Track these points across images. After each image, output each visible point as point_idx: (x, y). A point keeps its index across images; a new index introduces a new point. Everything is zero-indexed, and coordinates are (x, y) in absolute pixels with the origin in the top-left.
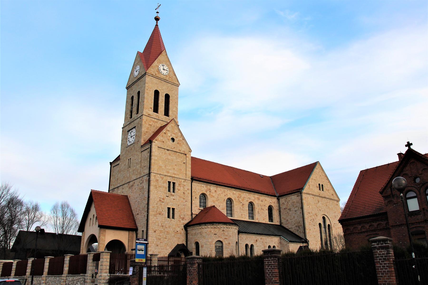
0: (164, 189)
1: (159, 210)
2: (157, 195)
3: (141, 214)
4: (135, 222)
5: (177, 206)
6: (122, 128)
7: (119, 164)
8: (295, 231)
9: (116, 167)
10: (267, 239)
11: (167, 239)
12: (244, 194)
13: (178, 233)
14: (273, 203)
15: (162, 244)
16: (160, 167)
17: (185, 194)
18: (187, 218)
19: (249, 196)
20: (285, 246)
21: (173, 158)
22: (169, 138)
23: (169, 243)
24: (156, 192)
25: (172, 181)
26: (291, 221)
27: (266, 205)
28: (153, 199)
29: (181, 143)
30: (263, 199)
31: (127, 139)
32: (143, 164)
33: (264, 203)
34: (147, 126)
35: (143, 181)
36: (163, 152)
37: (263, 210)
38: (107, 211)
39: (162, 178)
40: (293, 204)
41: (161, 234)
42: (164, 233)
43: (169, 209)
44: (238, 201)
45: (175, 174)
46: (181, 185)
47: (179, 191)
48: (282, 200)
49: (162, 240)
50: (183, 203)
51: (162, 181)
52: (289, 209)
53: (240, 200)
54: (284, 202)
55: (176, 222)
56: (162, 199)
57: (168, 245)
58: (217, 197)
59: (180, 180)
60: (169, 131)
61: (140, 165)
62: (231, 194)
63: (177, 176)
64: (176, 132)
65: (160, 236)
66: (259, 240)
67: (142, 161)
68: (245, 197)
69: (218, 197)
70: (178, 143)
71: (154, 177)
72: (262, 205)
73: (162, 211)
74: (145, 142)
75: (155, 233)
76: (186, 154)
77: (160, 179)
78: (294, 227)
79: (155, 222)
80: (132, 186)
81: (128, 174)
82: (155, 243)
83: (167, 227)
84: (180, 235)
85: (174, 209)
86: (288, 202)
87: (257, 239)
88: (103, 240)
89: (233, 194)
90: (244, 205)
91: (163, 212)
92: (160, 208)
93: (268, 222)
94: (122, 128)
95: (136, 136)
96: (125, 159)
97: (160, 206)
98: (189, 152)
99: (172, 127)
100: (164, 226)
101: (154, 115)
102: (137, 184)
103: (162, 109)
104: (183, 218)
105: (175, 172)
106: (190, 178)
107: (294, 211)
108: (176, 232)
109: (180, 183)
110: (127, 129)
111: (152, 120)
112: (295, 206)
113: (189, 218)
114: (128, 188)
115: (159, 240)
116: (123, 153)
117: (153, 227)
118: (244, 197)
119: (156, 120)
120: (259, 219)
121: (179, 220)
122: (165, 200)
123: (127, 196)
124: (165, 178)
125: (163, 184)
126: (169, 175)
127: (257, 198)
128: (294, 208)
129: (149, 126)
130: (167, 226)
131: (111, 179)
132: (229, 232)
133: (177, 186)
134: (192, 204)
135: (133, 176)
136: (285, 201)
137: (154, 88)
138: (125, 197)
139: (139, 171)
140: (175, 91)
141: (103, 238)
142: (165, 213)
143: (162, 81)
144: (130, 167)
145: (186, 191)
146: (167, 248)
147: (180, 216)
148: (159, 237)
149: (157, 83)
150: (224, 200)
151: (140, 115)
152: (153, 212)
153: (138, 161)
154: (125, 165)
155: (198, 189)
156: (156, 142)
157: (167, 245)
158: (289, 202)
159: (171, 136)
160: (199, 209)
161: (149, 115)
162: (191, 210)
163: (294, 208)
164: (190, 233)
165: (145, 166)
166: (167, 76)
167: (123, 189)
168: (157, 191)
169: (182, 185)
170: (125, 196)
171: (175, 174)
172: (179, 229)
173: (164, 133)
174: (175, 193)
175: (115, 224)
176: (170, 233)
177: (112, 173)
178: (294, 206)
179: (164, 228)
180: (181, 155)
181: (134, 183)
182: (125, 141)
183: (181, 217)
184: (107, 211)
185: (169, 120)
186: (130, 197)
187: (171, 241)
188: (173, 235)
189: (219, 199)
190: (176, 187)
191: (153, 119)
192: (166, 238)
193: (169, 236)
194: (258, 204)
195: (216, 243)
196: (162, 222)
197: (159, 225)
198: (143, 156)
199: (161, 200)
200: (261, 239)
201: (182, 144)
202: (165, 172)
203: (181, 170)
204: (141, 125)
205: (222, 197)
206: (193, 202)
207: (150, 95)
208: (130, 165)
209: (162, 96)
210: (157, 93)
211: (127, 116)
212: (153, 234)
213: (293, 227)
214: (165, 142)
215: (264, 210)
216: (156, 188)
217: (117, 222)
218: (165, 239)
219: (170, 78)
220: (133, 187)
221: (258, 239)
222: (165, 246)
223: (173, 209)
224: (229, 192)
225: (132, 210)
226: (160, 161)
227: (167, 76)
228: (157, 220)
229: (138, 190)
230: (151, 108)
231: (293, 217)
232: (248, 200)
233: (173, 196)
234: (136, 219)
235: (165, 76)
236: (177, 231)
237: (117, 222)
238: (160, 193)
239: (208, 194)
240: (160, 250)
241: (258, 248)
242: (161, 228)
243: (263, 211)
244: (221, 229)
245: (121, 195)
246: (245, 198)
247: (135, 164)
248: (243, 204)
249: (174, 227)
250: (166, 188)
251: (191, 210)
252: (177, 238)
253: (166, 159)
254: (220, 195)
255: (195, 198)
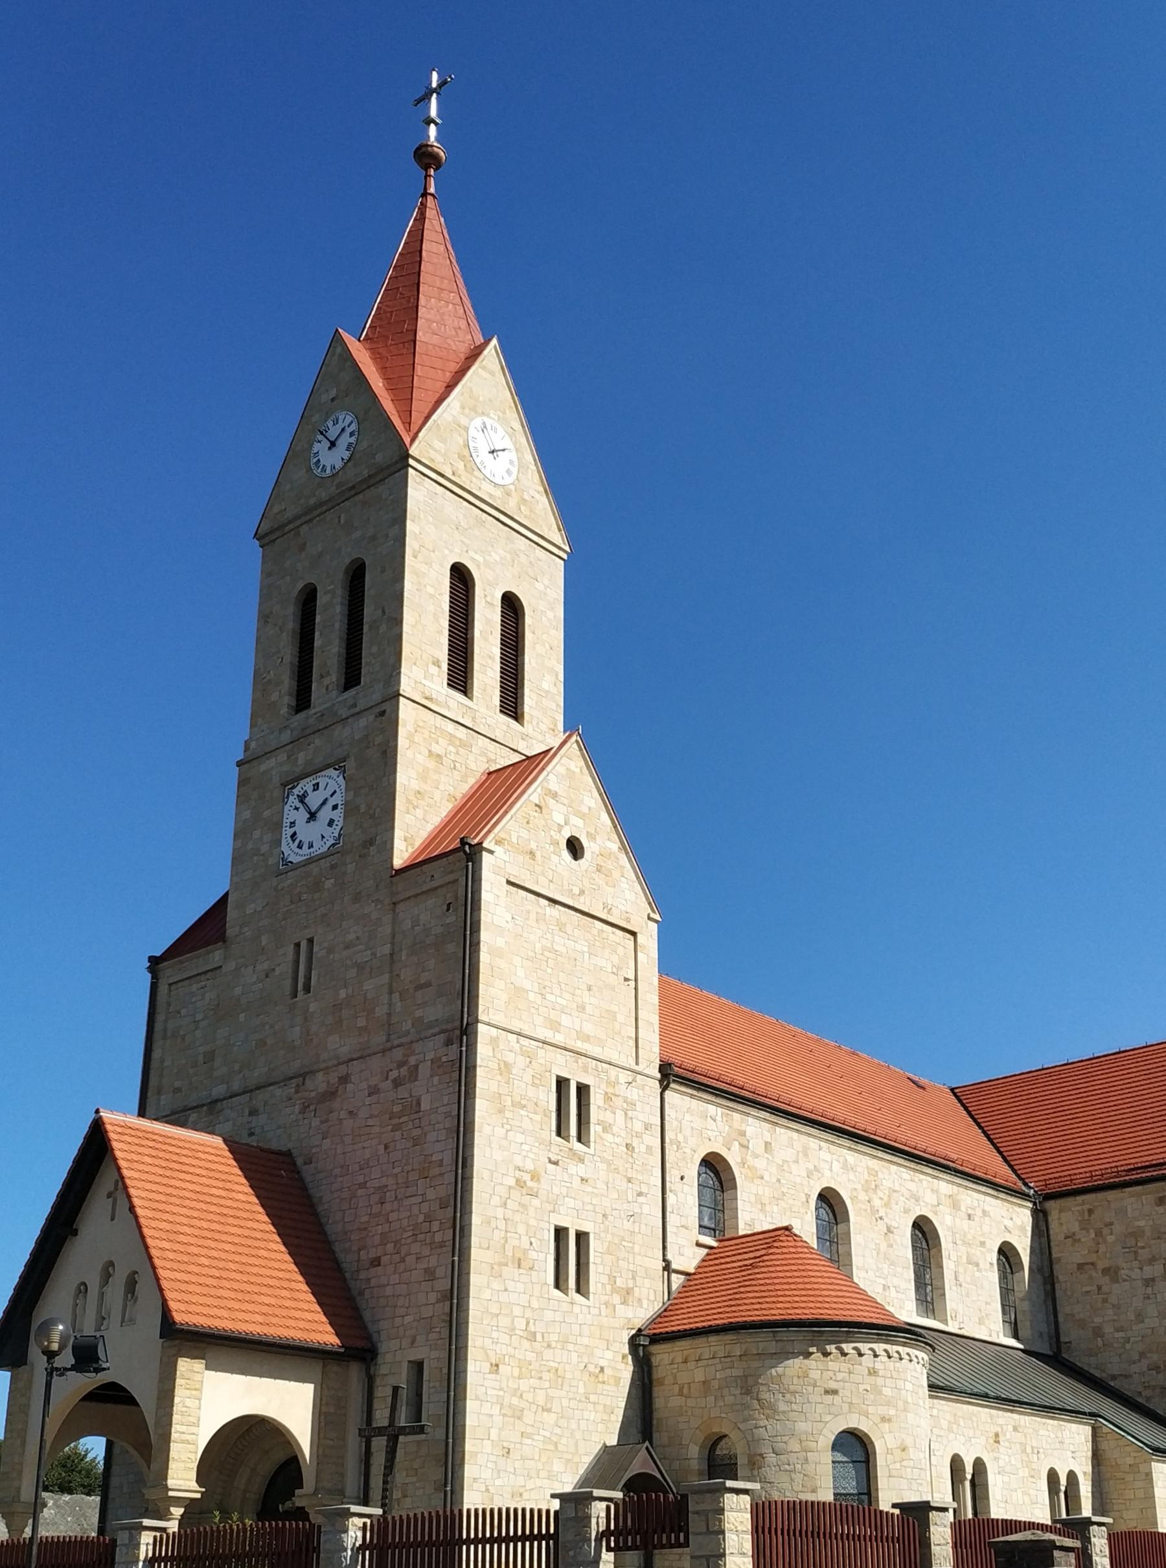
0: (537, 1118)
1: (512, 1241)
2: (506, 1153)
3: (403, 1260)
4: (356, 1309)
5: (600, 1218)
6: (239, 764)
7: (221, 966)
8: (1146, 1393)
9: (194, 987)
10: (1042, 1432)
11: (554, 1416)
12: (890, 1174)
13: (606, 1379)
14: (1017, 1232)
15: (529, 1441)
16: (519, 991)
17: (636, 1150)
18: (644, 1291)
19: (912, 1186)
20: (1129, 1478)
21: (579, 948)
22: (556, 836)
23: (564, 1441)
24: (499, 1131)
25: (575, 1077)
26: (1121, 1334)
27: (988, 1242)
28: (486, 1174)
29: (610, 871)
30: (974, 1209)
31: (278, 826)
32: (406, 974)
33: (978, 1229)
34: (420, 758)
35: (416, 1067)
36: (528, 912)
37: (977, 1265)
38: (201, 1242)
39: (531, 1057)
40: (1131, 1242)
41: (524, 1385)
42: (541, 1378)
43: (560, 1233)
44: (869, 1211)
45: (587, 1038)
46: (618, 1102)
47: (605, 1136)
48: (1064, 1217)
49: (528, 1417)
50: (625, 1206)
51: (530, 1072)
52: (1106, 1271)
53: (877, 1203)
54: (1075, 1227)
55: (596, 1311)
56: (526, 1177)
57: (560, 1447)
58: (774, 1180)
59: (613, 1071)
60: (555, 795)
61: (387, 976)
62: (836, 1166)
63: (596, 1051)
64: (589, 808)
65: (521, 1396)
66: (1008, 1436)
67: (404, 953)
68: (897, 1188)
69: (779, 1181)
70: (599, 869)
71: (491, 1048)
72: (970, 1237)
73: (527, 1246)
74: (411, 850)
75: (498, 1377)
76: (634, 934)
77: (521, 1061)
78: (1143, 1374)
79: (494, 1309)
80: (331, 1094)
81: (298, 1029)
82: (494, 1434)
83: (553, 1344)
84: (615, 1389)
85: (586, 1234)
86: (1099, 1233)
87: (999, 1429)
88: (192, 1419)
89: (845, 1166)
90: (892, 1233)
91: (533, 1255)
92: (521, 1229)
93: (1001, 1335)
94: (239, 764)
95: (350, 810)
96: (264, 940)
97: (517, 1218)
98: (646, 924)
99: (570, 774)
100: (539, 1338)
101: (452, 703)
102: (364, 1085)
103: (490, 673)
104: (629, 1291)
105: (589, 1029)
106: (658, 1066)
107: (1140, 1283)
108: (597, 1371)
109: (610, 1090)
110: (274, 766)
111: (442, 731)
112: (1144, 1254)
113: (655, 1291)
114: (297, 1109)
115: (517, 1421)
116: (253, 906)
117: (488, 1342)
118: (895, 1191)
119: (461, 733)
120: (959, 1319)
121: (606, 1304)
122: (542, 1180)
123: (289, 1154)
124: (545, 1055)
125: (531, 1092)
126: (559, 1039)
127: (945, 1195)
128: (1141, 1269)
129: (431, 764)
130: (554, 1338)
131: (156, 1054)
132: (900, 1383)
133: (599, 1107)
134: (668, 1214)
135: (333, 1041)
136: (1081, 1222)
137: (447, 552)
138: (272, 1156)
139: (381, 1011)
140: (546, 582)
141: (188, 1402)
142: (542, 1256)
143: (484, 514)
144: (307, 988)
145: (639, 1135)
146: (555, 1468)
147: (612, 1279)
148: (515, 1401)
149: (462, 524)
150: (808, 1196)
151: (377, 697)
152: (488, 1248)
153: (374, 954)
154: (267, 976)
155: (692, 1128)
156: (498, 850)
157: (552, 1448)
158: (1105, 1231)
159: (566, 824)
160: (698, 1245)
161: (427, 698)
162: (664, 1248)
163: (1136, 1264)
164: (669, 1380)
165: (428, 984)
166: (508, 494)
167: (253, 1112)
168: (507, 1131)
169: (620, 1098)
170: (279, 1153)
171: (587, 1038)
172: (609, 1355)
173: (536, 805)
174: (589, 1147)
175: (260, 1319)
176: (568, 1375)
177: (160, 1018)
178: (1136, 1252)
179: (537, 1345)
180: (612, 937)
181: (345, 1079)
182: (268, 837)
183: (620, 1282)
184: (201, 1242)
185: (523, 739)
186: (308, 1162)
187: (574, 1426)
188: (581, 1390)
189: (784, 1194)
190: (594, 1114)
191: (450, 727)
192: (549, 1406)
193: (563, 1393)
194: (954, 1234)
195: (843, 1434)
196: (528, 1314)
197: (514, 1329)
198: (407, 925)
199: (525, 1182)
200: (1015, 1429)
201: (616, 874)
202: (539, 1020)
203: (613, 1016)
204: (385, 752)
205: (798, 1180)
206: (671, 1199)
207: (430, 590)
208: (308, 978)
209: (488, 599)
210: (461, 577)
211: (274, 697)
212: (486, 1383)
213: (1135, 1368)
214: (538, 854)
215: (981, 1266)
216: (501, 1111)
217: (265, 1309)
218: (545, 1413)
219: (523, 508)
220: (336, 1104)
221: (1001, 1426)
222: (544, 1459)
223: (582, 1237)
224: (828, 1157)
225: (332, 1238)
226: (517, 961)
227: (508, 494)
228: (504, 1297)
229: (370, 1122)
230: (437, 663)
231: (1131, 1316)
232: (911, 1204)
233: (582, 1161)
234: (361, 1293)
235: (498, 493)
236: (602, 1369)
237: (265, 1309)
238: (520, 1138)
239: (733, 1158)
240: (521, 1481)
241: (1006, 1479)
242: (526, 1344)
243: (977, 1274)
244: (861, 1364)
245: (257, 1147)
246: (895, 1194)
247: (353, 973)
248: (889, 1230)
249: (586, 1341)
250: (546, 1113)
251: (664, 1248)
252: (601, 1408)
253: (546, 953)
254: (789, 1167)
255: (678, 1179)
